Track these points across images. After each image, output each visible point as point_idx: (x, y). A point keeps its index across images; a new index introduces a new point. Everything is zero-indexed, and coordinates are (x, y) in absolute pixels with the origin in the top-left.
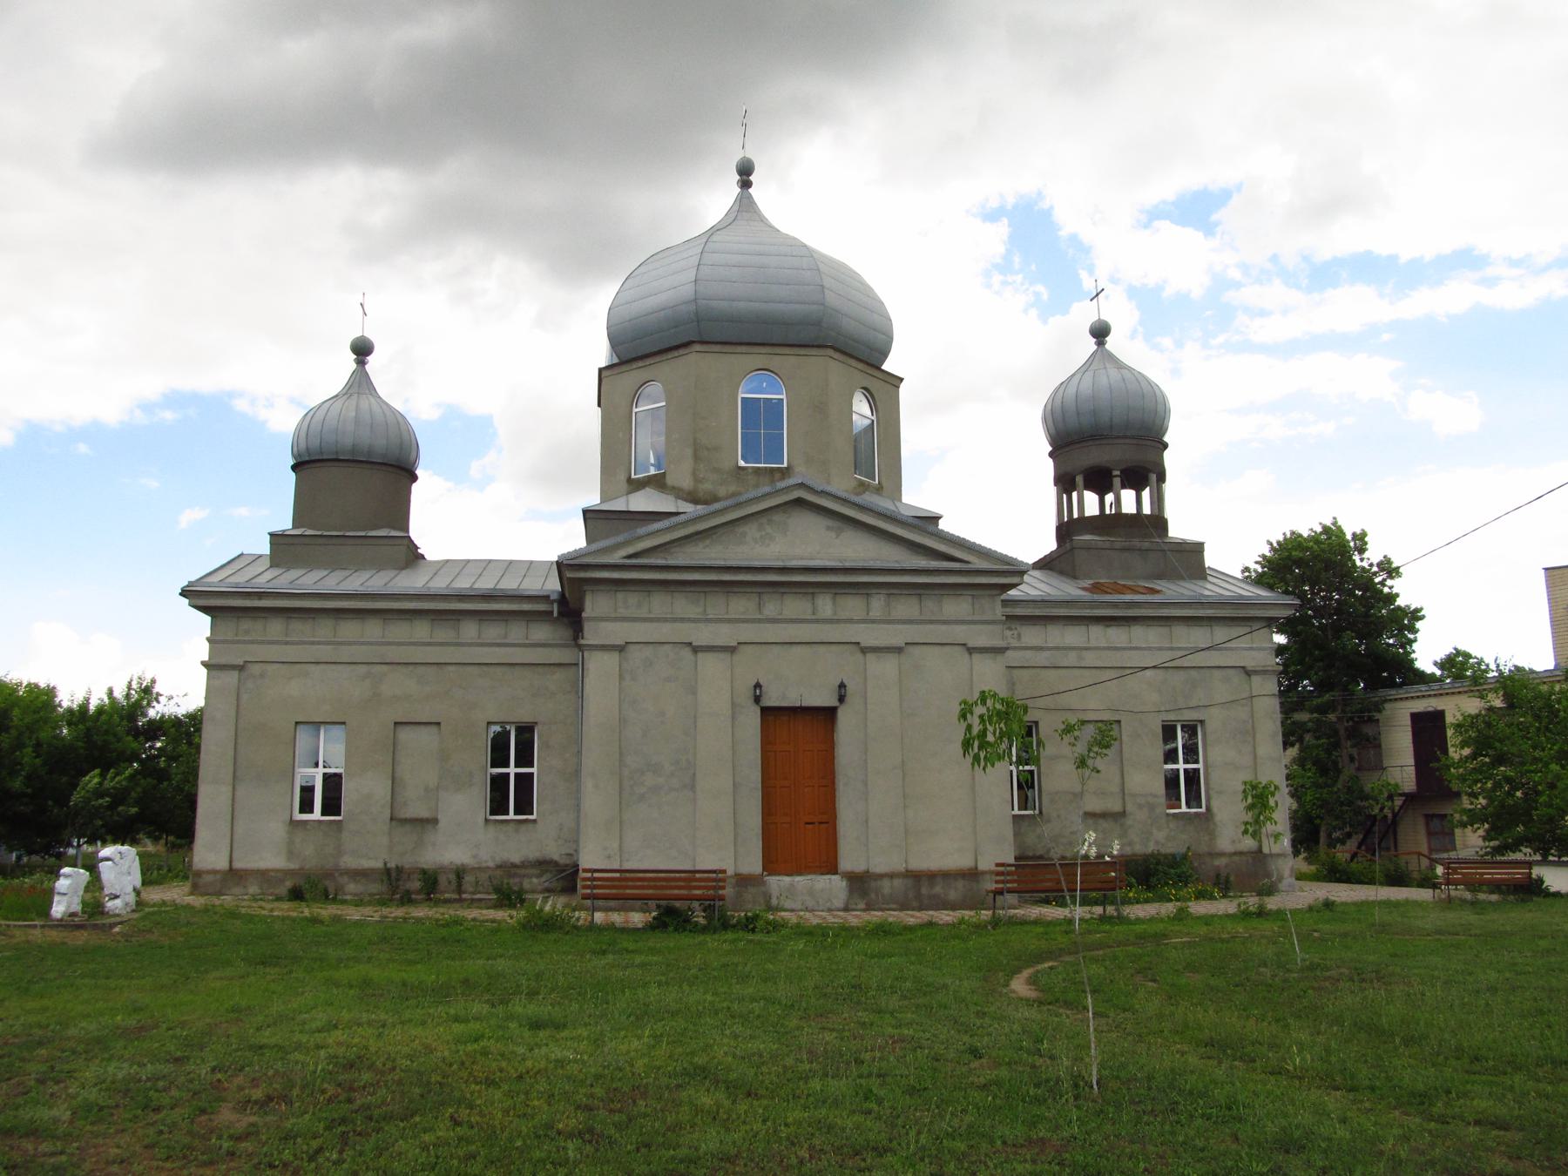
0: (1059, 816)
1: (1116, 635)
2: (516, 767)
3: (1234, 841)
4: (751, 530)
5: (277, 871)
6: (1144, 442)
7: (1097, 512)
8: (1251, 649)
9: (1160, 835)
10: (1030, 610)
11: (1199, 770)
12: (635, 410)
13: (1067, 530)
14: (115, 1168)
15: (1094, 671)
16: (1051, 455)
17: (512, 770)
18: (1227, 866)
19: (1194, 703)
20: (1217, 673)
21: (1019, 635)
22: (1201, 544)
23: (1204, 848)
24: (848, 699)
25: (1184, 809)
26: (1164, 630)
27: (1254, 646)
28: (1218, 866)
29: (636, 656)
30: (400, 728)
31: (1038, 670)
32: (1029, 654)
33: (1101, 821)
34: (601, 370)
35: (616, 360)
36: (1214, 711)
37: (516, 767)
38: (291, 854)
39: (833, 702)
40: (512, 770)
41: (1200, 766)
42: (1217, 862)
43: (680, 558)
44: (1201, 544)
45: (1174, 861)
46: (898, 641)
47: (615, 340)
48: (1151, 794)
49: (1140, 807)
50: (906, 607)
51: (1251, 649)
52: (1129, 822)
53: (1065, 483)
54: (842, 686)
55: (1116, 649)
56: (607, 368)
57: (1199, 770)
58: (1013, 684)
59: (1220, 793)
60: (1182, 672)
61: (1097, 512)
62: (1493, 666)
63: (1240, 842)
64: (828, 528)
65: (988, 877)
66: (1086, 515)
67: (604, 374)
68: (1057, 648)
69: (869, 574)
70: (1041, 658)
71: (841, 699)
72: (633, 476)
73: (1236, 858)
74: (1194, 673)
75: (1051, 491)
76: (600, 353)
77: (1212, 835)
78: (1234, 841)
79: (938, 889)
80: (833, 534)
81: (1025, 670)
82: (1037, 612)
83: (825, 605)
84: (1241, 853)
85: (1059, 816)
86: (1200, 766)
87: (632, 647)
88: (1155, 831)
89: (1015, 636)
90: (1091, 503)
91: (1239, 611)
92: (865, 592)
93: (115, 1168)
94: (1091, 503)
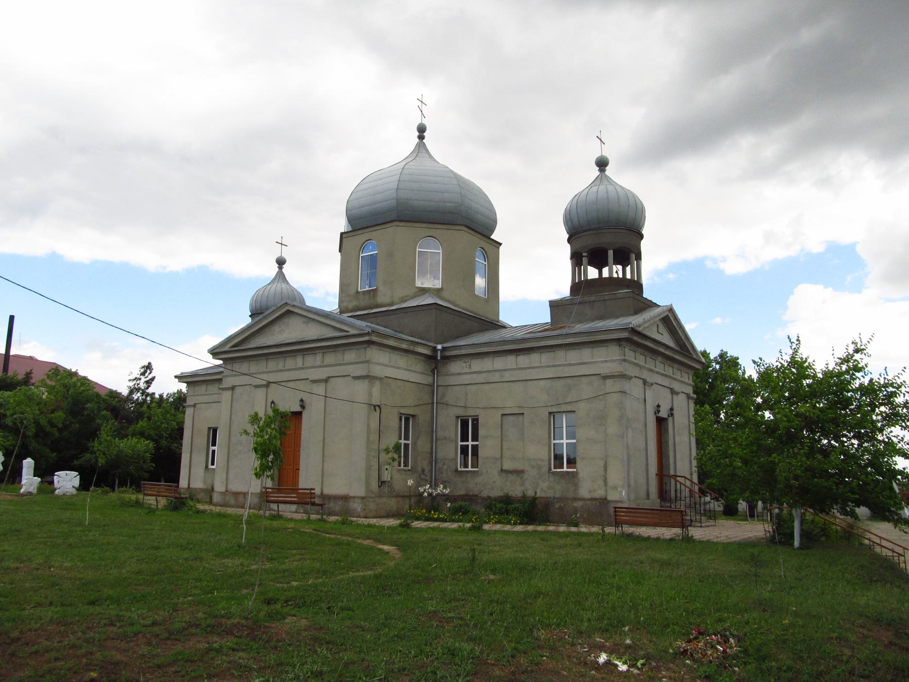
0: (487, 472)
1: (523, 360)
2: (567, 443)
3: (590, 491)
4: (276, 328)
5: (199, 489)
6: (602, 231)
7: (597, 276)
8: (606, 361)
9: (544, 485)
10: (468, 351)
11: (409, 444)
12: (361, 255)
13: (576, 288)
14: (523, 677)
15: (510, 383)
16: (569, 241)
17: (470, 443)
18: (582, 507)
19: (569, 400)
20: (584, 379)
21: (470, 365)
22: (549, 301)
23: (571, 495)
24: (307, 407)
25: (565, 469)
26: (551, 354)
27: (608, 359)
28: (576, 507)
29: (238, 390)
30: (505, 417)
31: (479, 385)
32: (474, 376)
33: (510, 475)
34: (342, 234)
35: (350, 229)
36: (582, 405)
37: (567, 443)
38: (205, 483)
39: (298, 409)
40: (470, 443)
41: (460, 443)
42: (576, 504)
43: (252, 344)
44: (549, 301)
45: (548, 504)
46: (324, 376)
47: (351, 219)
48: (540, 459)
49: (533, 467)
50: (330, 358)
51: (606, 361)
52: (526, 476)
53: (576, 258)
54: (302, 401)
55: (522, 369)
56: (345, 233)
57: (409, 444)
58: (467, 394)
59: (583, 459)
60: (562, 380)
61: (597, 276)
62: (743, 368)
63: (594, 491)
64: (304, 322)
65: (356, 500)
66: (589, 278)
67: (344, 236)
68: (488, 371)
69: (308, 343)
70: (481, 378)
71: (303, 407)
72: (359, 290)
73: (589, 502)
74: (569, 381)
75: (567, 264)
76: (342, 225)
77: (576, 486)
78: (590, 491)
79: (332, 505)
80: (305, 325)
81: (473, 386)
82: (472, 351)
83: (299, 361)
84: (595, 499)
85: (487, 472)
86: (460, 443)
87: (331, 380)
88: (541, 483)
89: (468, 366)
90: (592, 273)
91: (591, 337)
92: (313, 352)
93: (523, 677)
94: (592, 273)
